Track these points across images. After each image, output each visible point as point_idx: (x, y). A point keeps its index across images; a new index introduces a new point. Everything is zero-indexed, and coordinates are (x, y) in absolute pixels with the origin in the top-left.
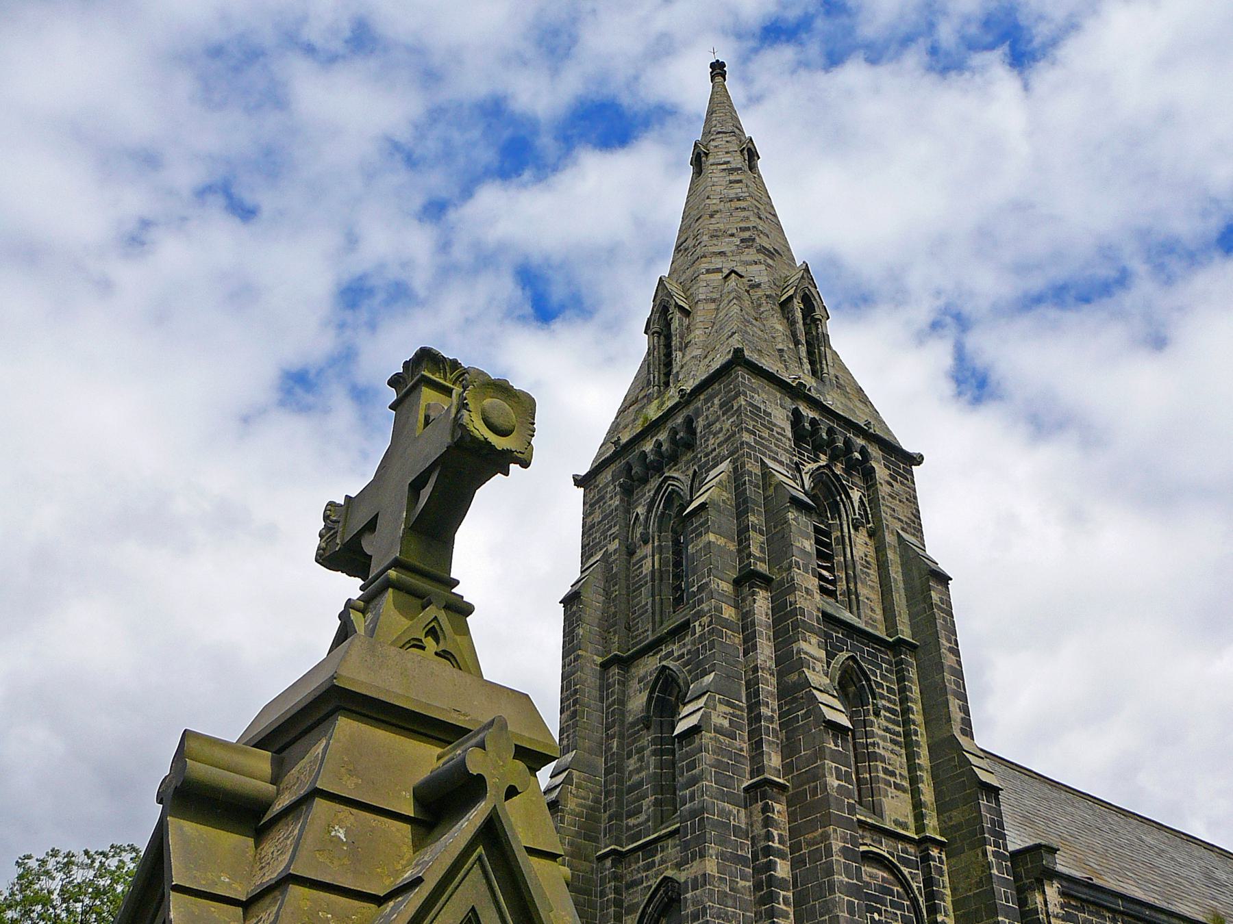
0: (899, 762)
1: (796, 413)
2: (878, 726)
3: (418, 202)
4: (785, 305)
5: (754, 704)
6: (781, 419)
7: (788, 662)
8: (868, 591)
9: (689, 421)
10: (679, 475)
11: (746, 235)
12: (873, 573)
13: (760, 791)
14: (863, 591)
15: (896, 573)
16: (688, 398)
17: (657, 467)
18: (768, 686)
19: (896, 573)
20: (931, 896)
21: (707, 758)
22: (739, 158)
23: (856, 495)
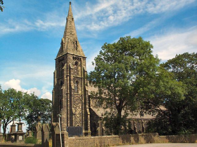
0: (81, 88)
1: (73, 57)
2: (79, 85)
3: (35, 92)
4: (74, 43)
5: (67, 87)
6: (72, 58)
7: (70, 83)
8: (80, 73)
9: (64, 57)
10: (63, 62)
11: (71, 32)
12: (80, 71)
13: (67, 94)
14: (79, 73)
15: (82, 71)
16: (63, 55)
17: (62, 60)
18: (68, 85)
19: (82, 71)
20: (82, 99)
21: (63, 91)
22: (71, 20)
23: (79, 63)
